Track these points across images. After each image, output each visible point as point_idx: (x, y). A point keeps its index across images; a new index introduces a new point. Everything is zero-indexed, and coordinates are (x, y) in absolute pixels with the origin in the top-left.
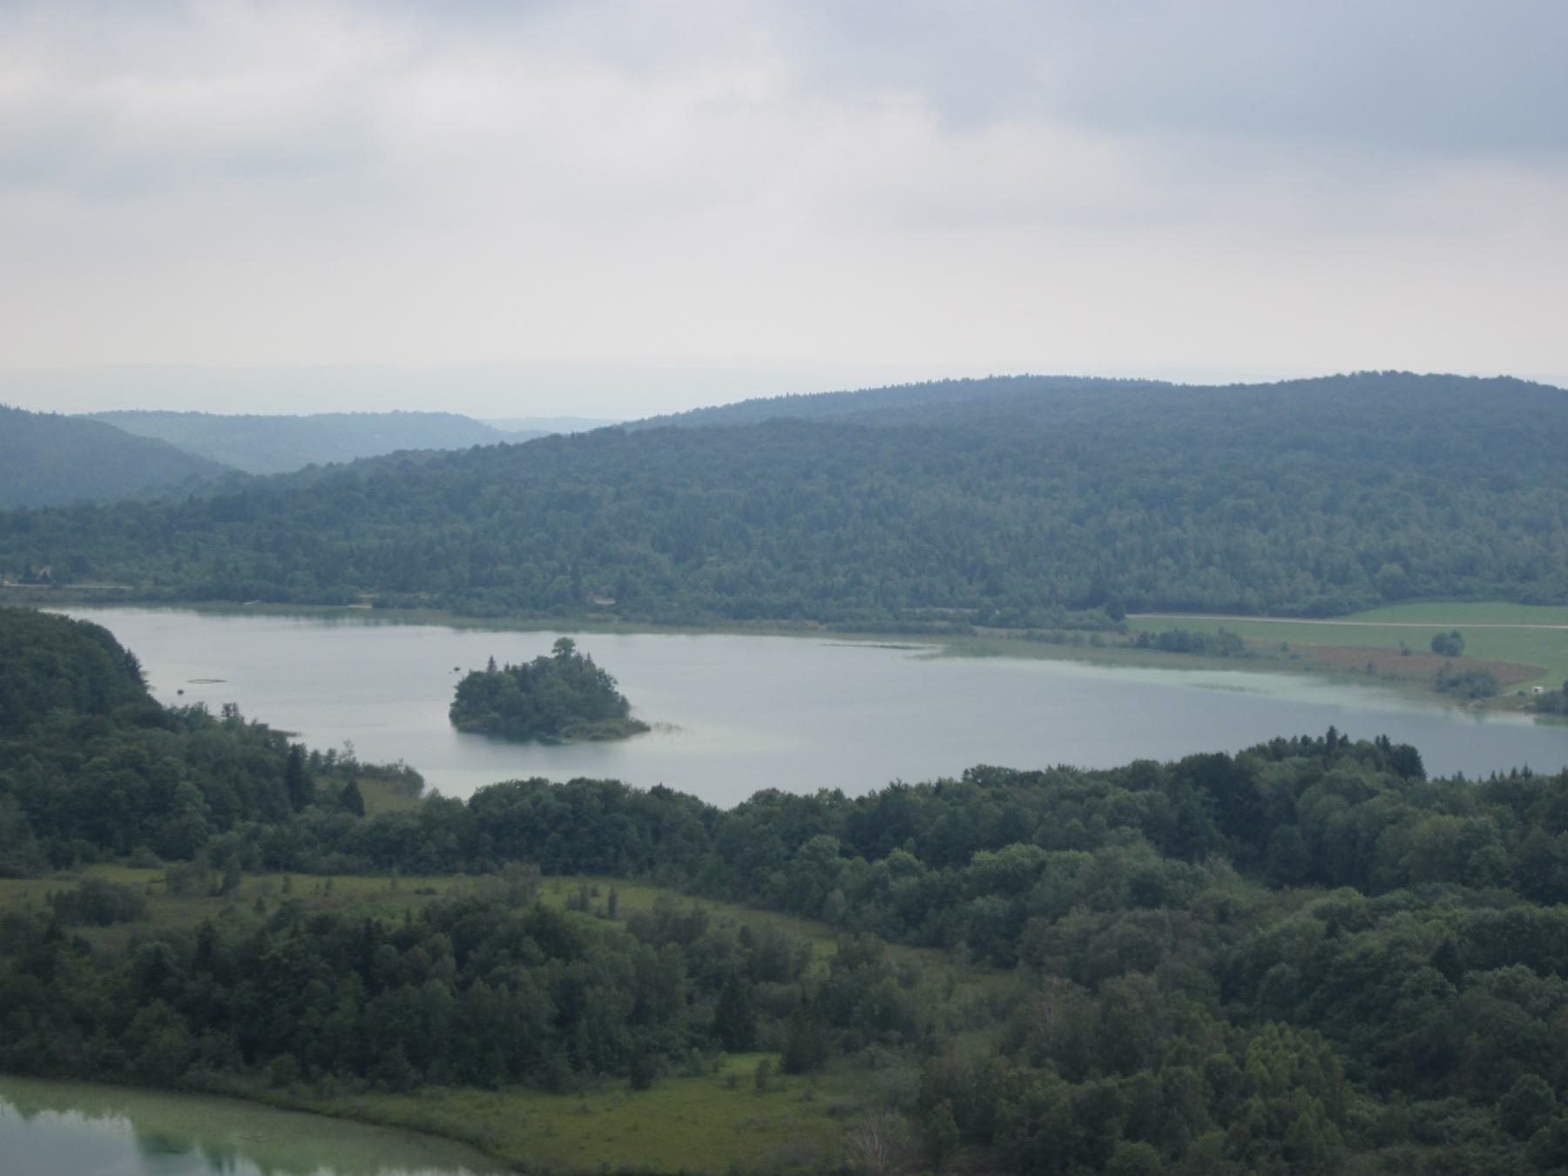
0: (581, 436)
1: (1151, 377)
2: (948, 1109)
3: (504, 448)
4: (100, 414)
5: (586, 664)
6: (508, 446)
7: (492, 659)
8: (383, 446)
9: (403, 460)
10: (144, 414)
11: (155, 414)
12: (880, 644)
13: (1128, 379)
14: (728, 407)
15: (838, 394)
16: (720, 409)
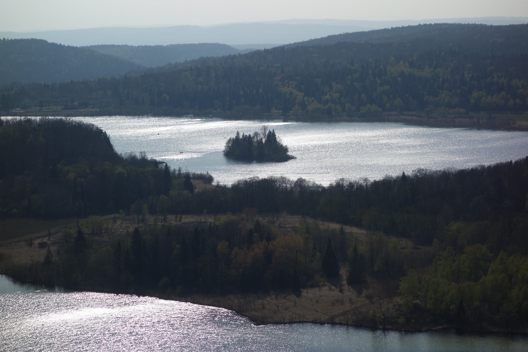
0: (268, 50)
1: (221, 42)
2: (49, 239)
3: (240, 56)
4: (91, 46)
5: (272, 134)
6: (242, 55)
7: (238, 132)
8: (196, 56)
9: (203, 61)
10: (107, 46)
11: (110, 45)
12: (185, 120)
13: (471, 23)
14: (322, 38)
15: (213, 44)
16: (319, 39)
